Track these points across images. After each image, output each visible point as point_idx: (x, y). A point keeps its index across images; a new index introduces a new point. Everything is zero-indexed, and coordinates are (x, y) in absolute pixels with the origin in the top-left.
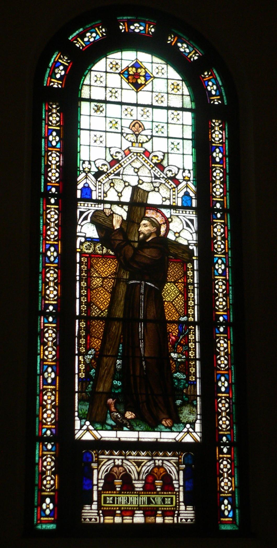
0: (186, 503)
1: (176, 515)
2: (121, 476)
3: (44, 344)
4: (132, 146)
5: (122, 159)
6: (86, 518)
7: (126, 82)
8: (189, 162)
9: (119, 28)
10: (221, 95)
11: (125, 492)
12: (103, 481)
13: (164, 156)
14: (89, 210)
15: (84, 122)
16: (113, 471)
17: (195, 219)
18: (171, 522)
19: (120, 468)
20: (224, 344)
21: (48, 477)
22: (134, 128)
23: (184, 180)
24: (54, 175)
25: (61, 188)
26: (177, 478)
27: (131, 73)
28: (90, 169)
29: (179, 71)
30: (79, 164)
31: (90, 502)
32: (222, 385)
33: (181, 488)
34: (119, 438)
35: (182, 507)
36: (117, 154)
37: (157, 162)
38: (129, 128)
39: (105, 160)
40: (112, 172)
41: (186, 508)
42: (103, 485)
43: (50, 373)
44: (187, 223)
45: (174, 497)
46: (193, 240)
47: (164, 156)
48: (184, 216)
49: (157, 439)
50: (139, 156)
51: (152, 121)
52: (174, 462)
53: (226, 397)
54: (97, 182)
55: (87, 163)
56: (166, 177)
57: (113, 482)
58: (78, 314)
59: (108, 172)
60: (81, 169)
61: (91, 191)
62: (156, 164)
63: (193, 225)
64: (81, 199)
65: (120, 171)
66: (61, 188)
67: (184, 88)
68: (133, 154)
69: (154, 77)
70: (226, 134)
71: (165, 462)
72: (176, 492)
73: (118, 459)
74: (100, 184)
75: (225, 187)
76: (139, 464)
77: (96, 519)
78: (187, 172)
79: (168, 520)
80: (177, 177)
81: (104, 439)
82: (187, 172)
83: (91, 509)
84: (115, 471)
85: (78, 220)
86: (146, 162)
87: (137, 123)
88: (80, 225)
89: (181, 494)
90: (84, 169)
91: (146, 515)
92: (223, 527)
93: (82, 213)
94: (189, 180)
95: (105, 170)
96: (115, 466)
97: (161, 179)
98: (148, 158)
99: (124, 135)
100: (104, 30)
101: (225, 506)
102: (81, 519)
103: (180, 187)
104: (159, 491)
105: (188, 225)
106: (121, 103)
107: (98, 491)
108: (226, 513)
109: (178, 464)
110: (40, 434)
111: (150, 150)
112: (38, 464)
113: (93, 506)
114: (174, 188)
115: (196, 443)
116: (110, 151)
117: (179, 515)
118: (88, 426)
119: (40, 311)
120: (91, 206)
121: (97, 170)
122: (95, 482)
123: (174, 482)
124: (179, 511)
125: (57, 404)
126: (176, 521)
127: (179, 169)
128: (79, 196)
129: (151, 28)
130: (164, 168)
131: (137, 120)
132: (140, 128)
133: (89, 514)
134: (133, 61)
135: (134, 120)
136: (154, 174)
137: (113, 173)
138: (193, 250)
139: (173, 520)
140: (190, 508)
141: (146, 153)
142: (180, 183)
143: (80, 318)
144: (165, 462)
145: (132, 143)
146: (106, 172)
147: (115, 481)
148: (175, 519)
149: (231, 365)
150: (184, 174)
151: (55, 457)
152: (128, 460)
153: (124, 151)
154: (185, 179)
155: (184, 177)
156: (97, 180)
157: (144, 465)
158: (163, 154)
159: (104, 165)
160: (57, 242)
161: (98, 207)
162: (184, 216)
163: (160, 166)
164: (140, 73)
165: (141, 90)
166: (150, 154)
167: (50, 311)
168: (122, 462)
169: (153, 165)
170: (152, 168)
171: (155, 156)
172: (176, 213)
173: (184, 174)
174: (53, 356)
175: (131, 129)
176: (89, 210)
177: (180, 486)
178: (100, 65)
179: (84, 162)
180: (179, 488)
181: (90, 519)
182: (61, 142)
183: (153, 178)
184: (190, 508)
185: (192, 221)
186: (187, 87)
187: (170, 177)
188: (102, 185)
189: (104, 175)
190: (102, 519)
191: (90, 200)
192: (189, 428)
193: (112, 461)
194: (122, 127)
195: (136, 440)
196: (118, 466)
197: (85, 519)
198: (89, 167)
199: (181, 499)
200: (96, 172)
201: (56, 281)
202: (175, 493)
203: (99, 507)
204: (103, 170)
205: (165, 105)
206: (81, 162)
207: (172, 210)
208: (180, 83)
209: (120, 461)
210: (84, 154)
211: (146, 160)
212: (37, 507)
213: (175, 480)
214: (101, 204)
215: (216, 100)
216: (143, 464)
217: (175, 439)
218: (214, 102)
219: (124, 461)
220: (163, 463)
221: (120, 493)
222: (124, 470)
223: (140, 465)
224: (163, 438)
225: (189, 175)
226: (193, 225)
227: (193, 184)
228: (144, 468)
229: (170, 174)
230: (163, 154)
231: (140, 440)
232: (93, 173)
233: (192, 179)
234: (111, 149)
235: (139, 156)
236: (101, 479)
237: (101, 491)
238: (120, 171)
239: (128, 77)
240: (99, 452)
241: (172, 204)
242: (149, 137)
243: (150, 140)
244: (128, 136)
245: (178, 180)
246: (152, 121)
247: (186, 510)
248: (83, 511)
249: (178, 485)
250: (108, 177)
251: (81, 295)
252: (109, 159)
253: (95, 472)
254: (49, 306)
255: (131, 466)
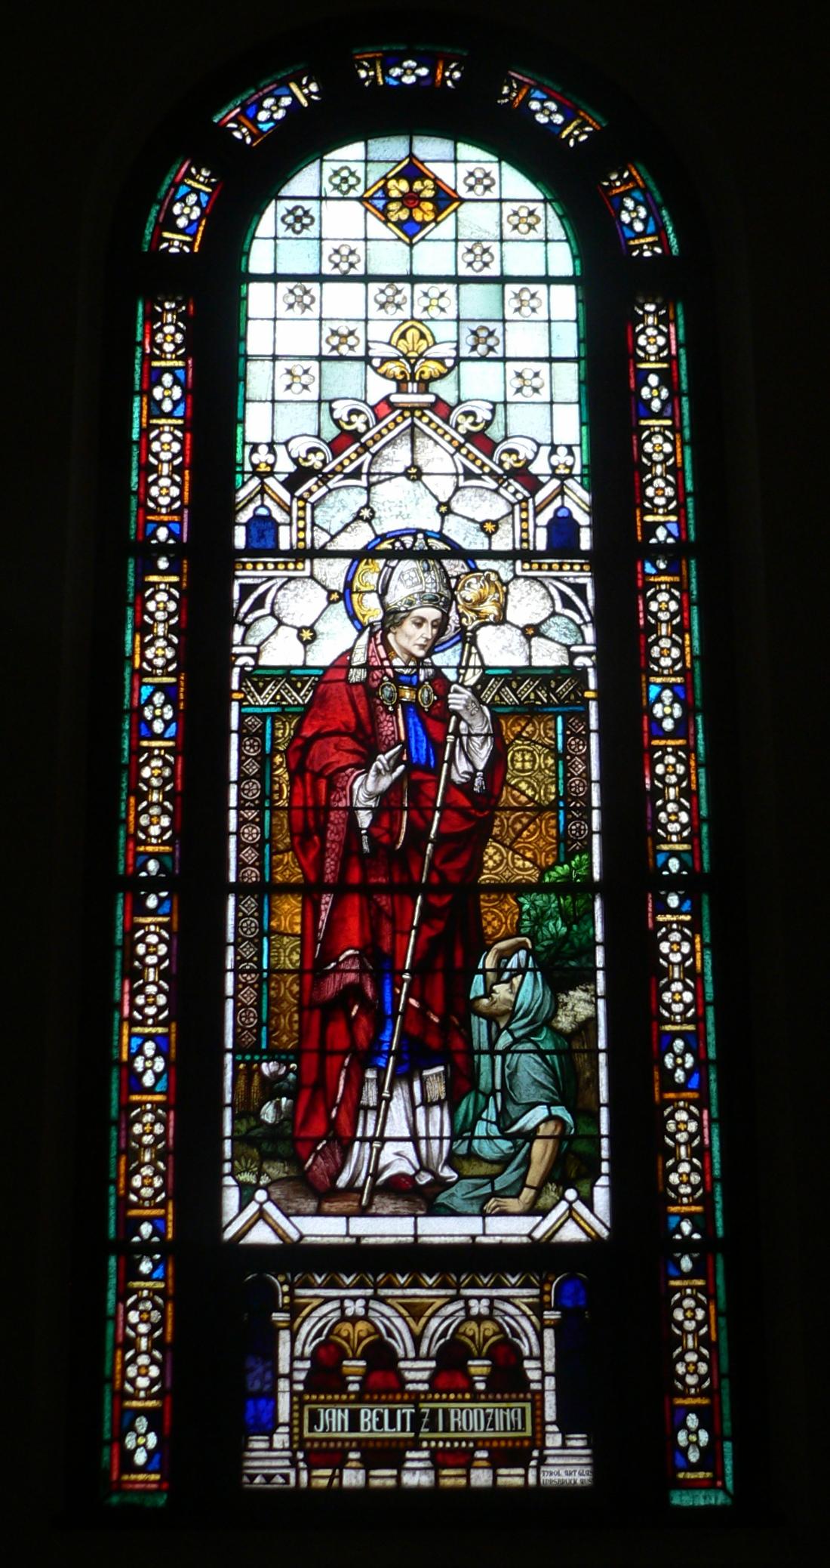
0: (566, 1426)
1: (533, 1463)
2: (364, 1347)
3: (143, 629)
4: (399, 391)
5: (368, 429)
6: (256, 1475)
7: (379, 219)
8: (569, 426)
9: (358, 75)
10: (660, 230)
11: (376, 1397)
12: (307, 1365)
13: (493, 412)
14: (270, 578)
15: (257, 339)
16: (338, 1335)
17: (587, 580)
18: (519, 1481)
19: (362, 1326)
20: (678, 766)
21: (163, 618)
22: (402, 341)
23: (554, 475)
24: (166, 447)
25: (167, 1416)
26: (536, 1351)
27: (394, 194)
28: (272, 466)
29: (534, 175)
30: (241, 454)
31: (269, 1427)
32: (690, 1443)
33: (550, 1383)
34: (359, 1238)
35: (554, 1440)
36: (354, 418)
37: (474, 429)
38: (389, 344)
39: (318, 436)
40: (339, 469)
41: (564, 1440)
42: (308, 1376)
43: (152, 1059)
44: (562, 594)
45: (528, 1406)
46: (584, 643)
47: (493, 412)
48: (557, 579)
49: (473, 1237)
50: (420, 418)
51: (458, 320)
52: (528, 1305)
53: (676, 748)
54: (295, 500)
55: (263, 449)
56: (500, 471)
57: (340, 1366)
58: (232, 878)
59: (326, 470)
60: (248, 468)
61: (276, 525)
62: (469, 436)
63: (585, 601)
64: (249, 551)
65: (360, 466)
66: (167, 1416)
67: (549, 218)
68: (401, 414)
69: (462, 201)
70: (677, 332)
71: (498, 1304)
72: (535, 1392)
73: (354, 1299)
74: (301, 504)
75: (680, 482)
76: (415, 1311)
77: (286, 1477)
78: (563, 451)
79: (511, 1477)
80: (534, 469)
81: (309, 1240)
82: (563, 451)
83: (271, 1449)
84: (345, 1334)
85: (235, 606)
86: (440, 431)
87: (412, 327)
88: (242, 623)
89: (550, 1399)
90: (255, 466)
91: (439, 1460)
92: (680, 1499)
93: (246, 590)
94: (571, 476)
95: (318, 465)
96: (344, 1318)
97: (486, 478)
98: (446, 421)
99: (376, 362)
100: (313, 88)
101: (676, 1056)
102: (241, 1478)
103: (541, 496)
104: (481, 1392)
105: (568, 603)
106: (367, 279)
107: (293, 1393)
108: (667, 695)
109: (538, 1308)
110: (136, 702)
111: (451, 400)
112: (115, 1318)
113: (276, 1437)
114: (525, 499)
115: (596, 1241)
116: (332, 410)
117: (542, 1460)
118: (261, 1204)
119: (121, 877)
120: (276, 569)
121: (292, 468)
122: (284, 1367)
123: (527, 1364)
124: (543, 1448)
125: (169, 1338)
126: (532, 1480)
127: (539, 445)
128: (240, 539)
129: (452, 71)
130: (496, 445)
131: (413, 319)
132: (423, 342)
133: (267, 1463)
134: (399, 162)
135: (405, 321)
136: (465, 467)
137: (341, 472)
138: (585, 668)
139: (526, 1476)
140: (577, 1441)
141: (441, 407)
142: (542, 485)
143: (241, 889)
144: (498, 1304)
145: (399, 383)
146: (320, 471)
147: (345, 1363)
148: (532, 1473)
149: (721, 1376)
150: (555, 460)
151: (171, 803)
152: (383, 1300)
153: (373, 408)
154: (558, 472)
155: (554, 468)
156: (293, 496)
157: (433, 1315)
158: (491, 407)
159: (313, 450)
160: (162, 1208)
161: (296, 569)
162: (557, 579)
163: (481, 440)
164: (421, 191)
165: (423, 239)
166: (452, 409)
167: (149, 877)
168: (367, 1308)
169: (462, 440)
170: (458, 449)
171: (467, 414)
172: (531, 569)
173: (555, 460)
174: (168, 660)
175: (396, 347)
176: (270, 578)
177: (544, 1374)
178: (304, 182)
179: (255, 448)
180: (542, 1381)
181: (269, 1478)
182: (189, 401)
183: (461, 478)
184: (577, 1441)
185: (580, 590)
186: (560, 217)
187: (512, 468)
188: (309, 506)
189: (315, 479)
190: (304, 1476)
191: (275, 552)
192: (574, 1201)
193: (335, 1304)
194: (367, 342)
195: (411, 1240)
196: (354, 1320)
197: (252, 1477)
198: (271, 459)
199: (550, 1413)
200: (290, 474)
201: (168, 788)
202: (529, 1396)
203: (298, 1442)
204: (312, 466)
205: (494, 271)
206: (248, 449)
207: (519, 563)
208: (539, 208)
209: (361, 1303)
210: (256, 425)
211: (439, 427)
212: (141, 393)
213: (531, 1358)
214: (303, 562)
215: (645, 247)
216: (429, 1313)
217: (529, 1235)
218: (642, 251)
219: (373, 1304)
220: (491, 1307)
221: (360, 1398)
222: (372, 1330)
223: (422, 1316)
224: (494, 1235)
225: (569, 461)
226: (585, 601)
227: (581, 484)
228: (434, 1323)
229: (509, 461)
230: (491, 407)
231: (422, 1240)
232: (282, 477)
233: (577, 470)
234: (334, 405)
235: (420, 418)
236: (302, 1358)
237: (300, 1394)
238: (360, 466)
239: (385, 206)
240: (296, 1279)
241: (518, 546)
242: (449, 363)
243: (450, 370)
244: (389, 366)
245: (536, 476)
246: (458, 320)
247: (564, 1446)
248: (248, 1454)
249: (540, 1372)
250: (325, 483)
251: (243, 776)
252: (330, 432)
253: (285, 1336)
254: (142, 1223)
255: (393, 1319)
